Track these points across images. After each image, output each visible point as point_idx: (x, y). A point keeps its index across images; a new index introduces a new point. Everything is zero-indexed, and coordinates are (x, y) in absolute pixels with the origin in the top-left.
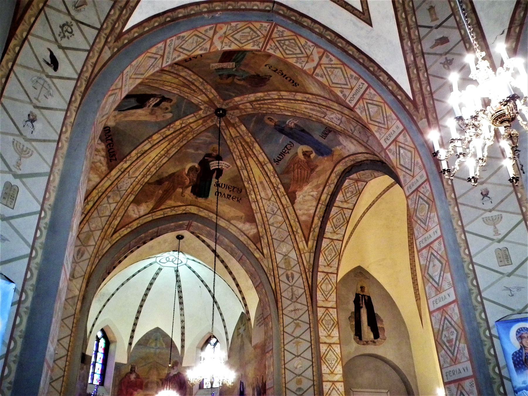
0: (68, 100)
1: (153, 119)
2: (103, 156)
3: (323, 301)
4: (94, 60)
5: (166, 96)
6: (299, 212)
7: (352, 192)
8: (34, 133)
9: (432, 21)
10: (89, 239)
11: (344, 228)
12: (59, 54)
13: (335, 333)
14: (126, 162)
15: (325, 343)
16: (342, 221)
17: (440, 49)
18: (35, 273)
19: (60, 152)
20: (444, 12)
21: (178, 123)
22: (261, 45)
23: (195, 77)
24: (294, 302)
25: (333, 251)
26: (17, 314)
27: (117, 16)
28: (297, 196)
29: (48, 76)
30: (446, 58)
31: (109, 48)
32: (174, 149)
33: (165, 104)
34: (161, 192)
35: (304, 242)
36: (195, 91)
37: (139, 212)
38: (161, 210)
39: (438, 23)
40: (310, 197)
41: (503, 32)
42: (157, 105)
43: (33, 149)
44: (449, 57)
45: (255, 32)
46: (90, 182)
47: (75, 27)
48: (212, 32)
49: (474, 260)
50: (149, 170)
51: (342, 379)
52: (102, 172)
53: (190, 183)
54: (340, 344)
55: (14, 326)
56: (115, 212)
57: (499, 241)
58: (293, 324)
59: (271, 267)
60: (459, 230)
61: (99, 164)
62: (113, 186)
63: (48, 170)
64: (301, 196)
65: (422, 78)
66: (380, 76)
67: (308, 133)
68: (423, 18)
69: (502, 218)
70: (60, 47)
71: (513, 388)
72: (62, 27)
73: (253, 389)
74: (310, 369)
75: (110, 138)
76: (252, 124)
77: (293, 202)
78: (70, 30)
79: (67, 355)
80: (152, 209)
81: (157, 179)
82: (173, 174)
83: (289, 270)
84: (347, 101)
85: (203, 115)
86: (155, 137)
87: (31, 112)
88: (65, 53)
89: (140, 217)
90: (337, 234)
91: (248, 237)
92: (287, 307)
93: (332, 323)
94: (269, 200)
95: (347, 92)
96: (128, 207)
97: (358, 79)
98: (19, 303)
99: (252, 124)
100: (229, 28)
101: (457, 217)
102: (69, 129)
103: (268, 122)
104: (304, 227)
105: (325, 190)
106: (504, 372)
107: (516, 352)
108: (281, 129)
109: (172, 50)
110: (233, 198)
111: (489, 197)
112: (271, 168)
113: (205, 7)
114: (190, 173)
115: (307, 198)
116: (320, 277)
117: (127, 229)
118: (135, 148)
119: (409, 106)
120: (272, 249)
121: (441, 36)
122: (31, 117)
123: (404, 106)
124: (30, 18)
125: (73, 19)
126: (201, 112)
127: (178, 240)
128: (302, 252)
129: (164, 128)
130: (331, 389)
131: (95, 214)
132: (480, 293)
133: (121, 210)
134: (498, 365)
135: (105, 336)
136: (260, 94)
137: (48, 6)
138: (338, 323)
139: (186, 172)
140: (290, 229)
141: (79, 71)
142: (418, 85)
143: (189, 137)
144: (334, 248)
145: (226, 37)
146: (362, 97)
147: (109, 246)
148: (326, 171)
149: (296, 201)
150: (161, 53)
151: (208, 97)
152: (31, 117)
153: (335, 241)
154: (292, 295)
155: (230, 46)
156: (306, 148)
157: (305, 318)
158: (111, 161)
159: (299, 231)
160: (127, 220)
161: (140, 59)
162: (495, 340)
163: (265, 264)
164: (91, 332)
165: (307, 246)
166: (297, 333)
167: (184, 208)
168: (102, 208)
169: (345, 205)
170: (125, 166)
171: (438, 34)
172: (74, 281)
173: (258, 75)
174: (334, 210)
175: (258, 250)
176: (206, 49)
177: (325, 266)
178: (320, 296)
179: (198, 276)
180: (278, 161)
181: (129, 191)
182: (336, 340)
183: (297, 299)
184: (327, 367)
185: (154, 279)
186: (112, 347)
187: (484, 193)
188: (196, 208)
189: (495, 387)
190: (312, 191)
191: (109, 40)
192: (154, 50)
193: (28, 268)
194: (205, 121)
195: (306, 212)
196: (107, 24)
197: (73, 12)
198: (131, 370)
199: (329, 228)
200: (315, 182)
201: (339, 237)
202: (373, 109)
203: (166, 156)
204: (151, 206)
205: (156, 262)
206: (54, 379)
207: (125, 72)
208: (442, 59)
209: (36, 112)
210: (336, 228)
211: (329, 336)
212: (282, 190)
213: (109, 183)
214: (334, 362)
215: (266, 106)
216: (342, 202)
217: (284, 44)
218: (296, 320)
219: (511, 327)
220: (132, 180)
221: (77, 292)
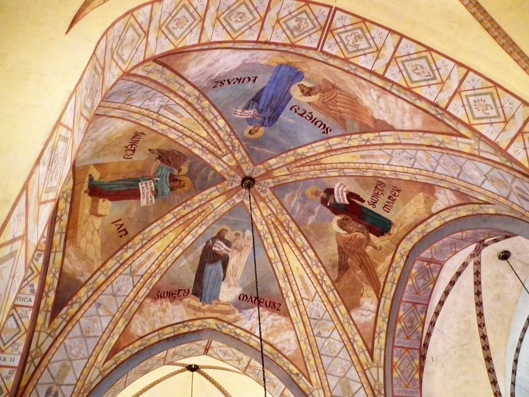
6: (407, 125)
7: (359, 37)
10: (349, 387)
11: (440, 61)
16: (423, 62)
25: (483, 97)
28: (382, 119)
32: (298, 240)
34: (359, 272)
37: (369, 310)
38: (385, 283)
40: (381, 100)
46: (291, 342)
50: (315, 276)
52: (286, 325)
53: (363, 233)
64: (381, 112)
75: (253, 299)
77: (391, 129)
80: (377, 293)
81: (336, 269)
82: (340, 248)
90: (449, 78)
104: (434, 129)
110: (394, 195)
114: (347, 228)
117: (380, 337)
128: (477, 153)
139: (345, 232)
143: (286, 219)
144: (475, 95)
147: (381, 371)
148: (329, 70)
149: (389, 123)
153: (463, 88)
158: (278, 310)
160: (369, 330)
165: (468, 138)
167: (397, 256)
168: (327, 349)
169: (388, 52)
177: (504, 130)
180: (326, 130)
188: (404, 241)
201: (457, 74)
204: (372, 293)
210: (435, 78)
213: (301, 324)
216: (377, 58)
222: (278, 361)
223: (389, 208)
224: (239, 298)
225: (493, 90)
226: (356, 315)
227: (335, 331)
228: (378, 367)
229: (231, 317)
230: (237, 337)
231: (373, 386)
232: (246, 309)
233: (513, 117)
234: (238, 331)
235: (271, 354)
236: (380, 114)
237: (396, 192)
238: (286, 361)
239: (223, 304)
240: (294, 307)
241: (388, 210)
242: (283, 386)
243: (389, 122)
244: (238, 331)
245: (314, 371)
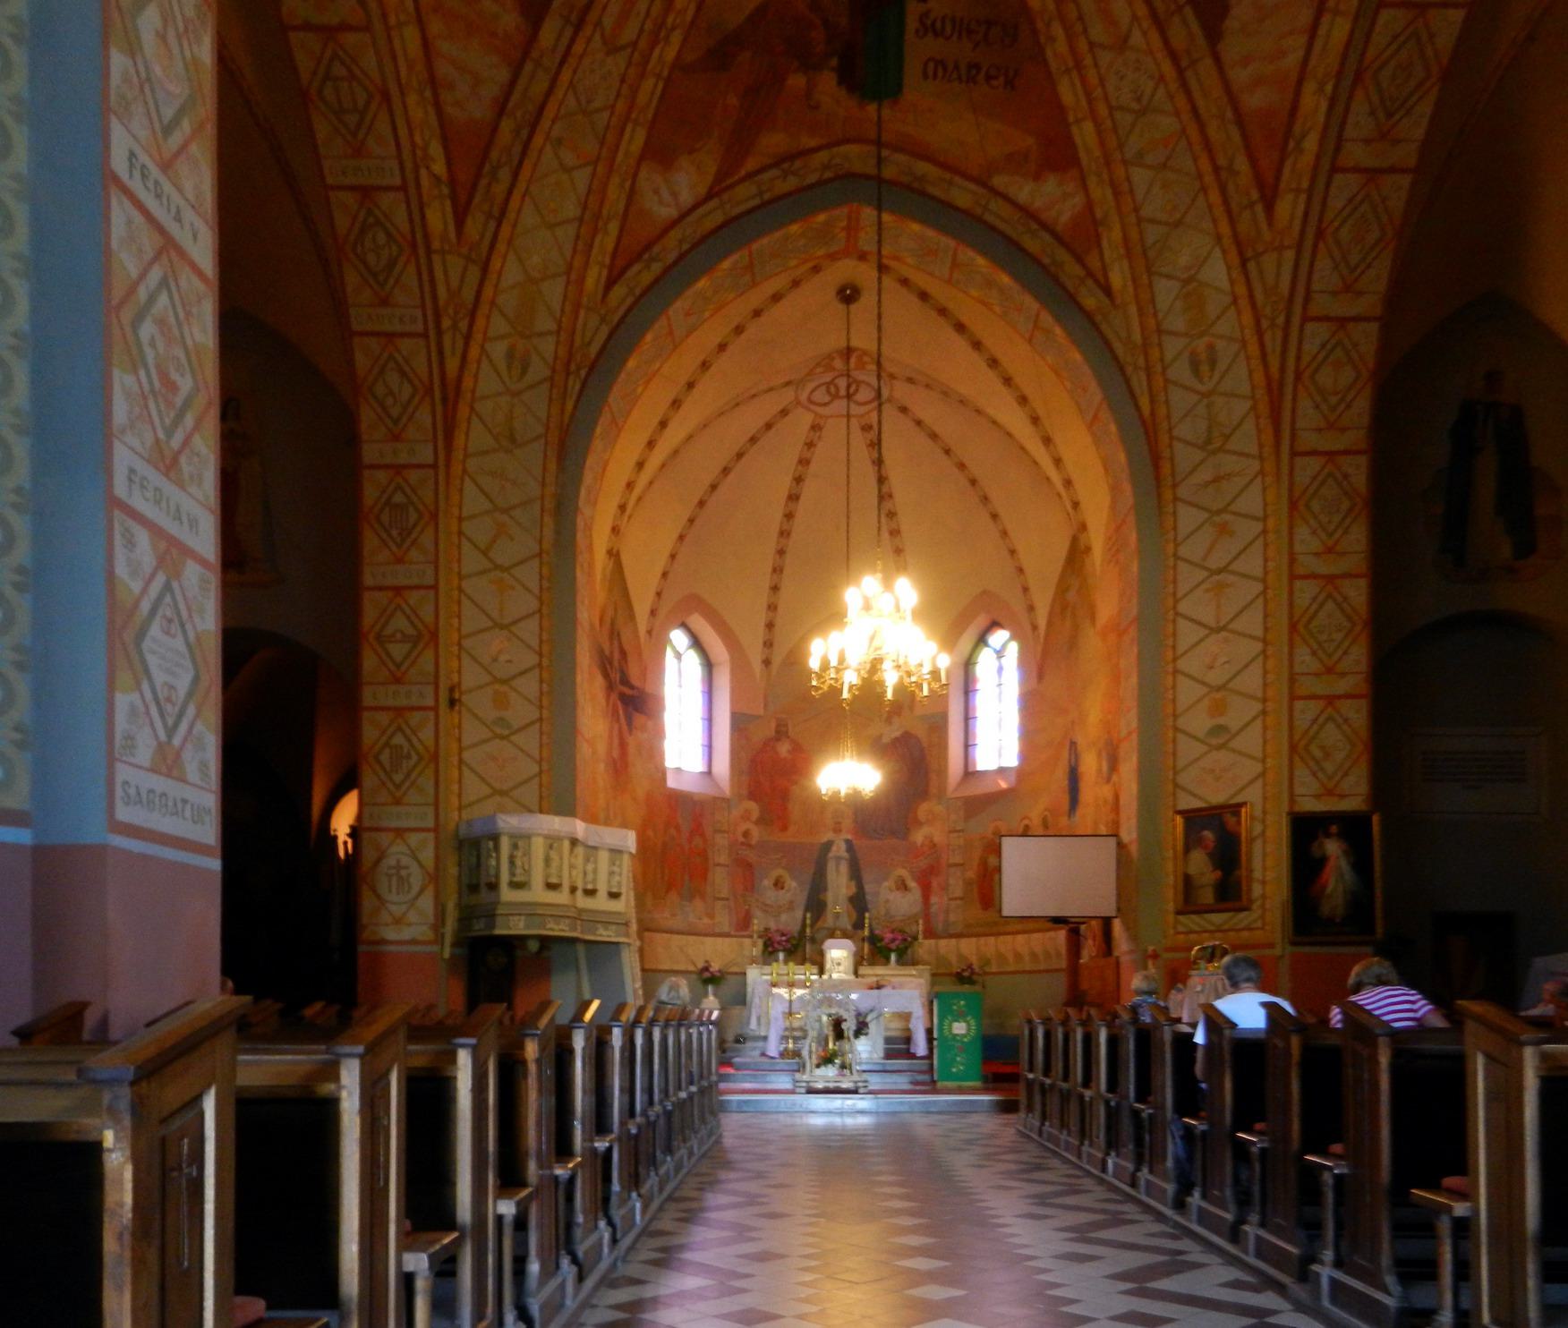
6: (1240, 76)
15: (1313, 576)
24: (1221, 449)
34: (733, 101)
35: (1259, 208)
38: (749, 176)
62: (559, 93)
73: (1099, 755)
74: (1256, 669)
79: (540, 665)
80: (720, 176)
83: (1202, 335)
91: (1053, 233)
92: (1191, 473)
94: (1122, 44)
96: (635, 176)
110: (989, 78)
127: (842, 307)
147: (604, 332)
167: (823, 156)
175: (1090, 282)
183: (1227, 437)
198: (777, 732)
204: (712, 168)
206: (516, 727)
218: (1219, 512)
223: (940, 73)
226: (649, 177)
227: (589, 169)
228: (603, 320)
230: (916, 185)
231: (441, 303)
233: (1360, 294)
237: (1002, 79)
241: (931, 73)
243: (1231, 24)
245: (489, 216)
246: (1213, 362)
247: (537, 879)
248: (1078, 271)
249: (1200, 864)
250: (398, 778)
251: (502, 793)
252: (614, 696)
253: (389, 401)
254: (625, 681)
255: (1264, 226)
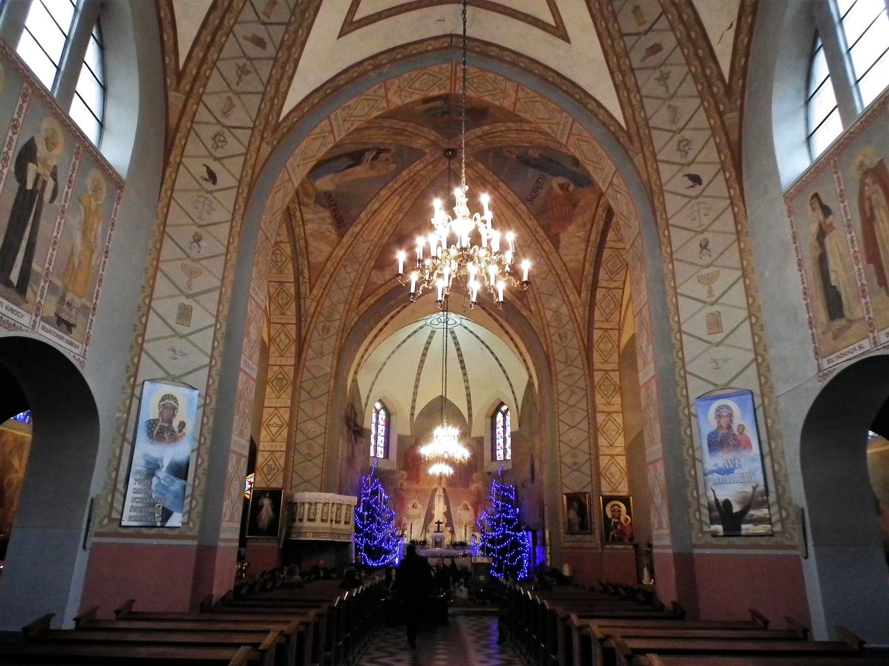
0: (231, 209)
1: (373, 174)
2: (330, 224)
3: (601, 363)
4: (252, 161)
5: (382, 148)
6: (566, 259)
8: (202, 252)
9: (640, 25)
12: (215, 167)
13: (617, 400)
14: (356, 226)
15: (603, 412)
17: (653, 60)
18: (217, 378)
19: (229, 265)
20: (651, 10)
21: (404, 173)
22: (448, 87)
23: (403, 124)
24: (570, 365)
25: (612, 302)
26: (204, 414)
27: (268, 109)
28: (561, 239)
29: (207, 192)
30: (661, 72)
31: (268, 144)
32: (407, 203)
33: (383, 156)
35: (576, 294)
36: (411, 137)
39: (647, 26)
40: (577, 239)
41: (731, 25)
42: (374, 159)
43: (201, 268)
44: (665, 69)
45: (436, 76)
47: (227, 134)
48: (383, 90)
49: (683, 328)
50: (385, 230)
51: (624, 453)
54: (622, 412)
55: (202, 425)
56: (356, 281)
57: (712, 304)
58: (569, 391)
59: (540, 326)
60: (671, 293)
61: (327, 233)
62: (348, 254)
63: (219, 283)
64: (566, 239)
65: (634, 102)
66: (588, 103)
67: (557, 163)
68: (629, 24)
69: (719, 275)
70: (216, 159)
71: (704, 470)
72: (214, 139)
76: (490, 160)
78: (222, 138)
79: (325, 432)
84: (558, 138)
85: (432, 160)
86: (382, 193)
87: (196, 233)
88: (222, 164)
89: (386, 283)
90: (615, 281)
93: (613, 388)
95: (555, 128)
96: (370, 274)
97: (562, 113)
98: (205, 405)
99: (490, 160)
100: (401, 80)
101: (670, 276)
102: (236, 239)
103: (508, 155)
105: (594, 229)
106: (697, 455)
107: (712, 432)
108: (527, 162)
109: (341, 123)
111: (708, 250)
112: (524, 208)
113: (369, 64)
115: (572, 240)
116: (597, 335)
118: (363, 210)
119: (623, 139)
120: (540, 305)
121: (653, 43)
122: (196, 237)
123: (617, 139)
124: (180, 141)
125: (224, 126)
126: (427, 157)
129: (390, 182)
130: (610, 463)
131: (334, 287)
132: (684, 367)
133: (362, 278)
134: (692, 446)
135: (384, 407)
136: (486, 128)
137: (198, 123)
138: (620, 387)
140: (558, 280)
141: (238, 177)
142: (630, 111)
145: (403, 90)
146: (570, 133)
150: (328, 129)
151: (430, 140)
152: (196, 237)
154: (567, 358)
155: (411, 97)
156: (561, 180)
157: (582, 383)
159: (569, 281)
161: (304, 144)
162: (693, 418)
163: (534, 322)
164: (366, 405)
166: (572, 402)
170: (357, 230)
171: (648, 41)
172: (324, 358)
173: (474, 108)
174: (606, 253)
176: (384, 108)
177: (602, 321)
178: (597, 359)
179: (477, 337)
180: (531, 200)
181: (368, 256)
182: (617, 407)
183: (572, 362)
184: (605, 439)
185: (428, 343)
186: (393, 419)
187: (703, 245)
189: (686, 469)
190: (578, 232)
191: (265, 135)
192: (317, 130)
193: (209, 376)
194: (434, 166)
195: (574, 258)
196: (260, 121)
197: (222, 120)
199: (602, 274)
200: (580, 220)
202: (585, 147)
203: (400, 212)
205: (426, 324)
207: (287, 164)
208: (657, 74)
209: (201, 231)
210: (612, 274)
211: (609, 403)
212: (542, 233)
213: (343, 251)
214: (613, 433)
215: (497, 139)
217: (473, 83)
219: (710, 405)
220: (368, 244)
221: (328, 370)
222: (300, 258)
224: (325, 193)
225: (618, 305)
229: (306, 200)
232: (320, 205)
233: (611, 322)
234: (298, 213)
235: (300, 249)
236: (564, 239)
238: (306, 263)
239: (313, 187)
240: (352, 236)
242: (660, 455)
244: (298, 213)
246: (566, 338)
247: (318, 517)
248: (520, 303)
249: (573, 515)
250: (269, 477)
251: (307, 482)
252: (351, 432)
253: (281, 344)
254: (355, 425)
255: (578, 299)
